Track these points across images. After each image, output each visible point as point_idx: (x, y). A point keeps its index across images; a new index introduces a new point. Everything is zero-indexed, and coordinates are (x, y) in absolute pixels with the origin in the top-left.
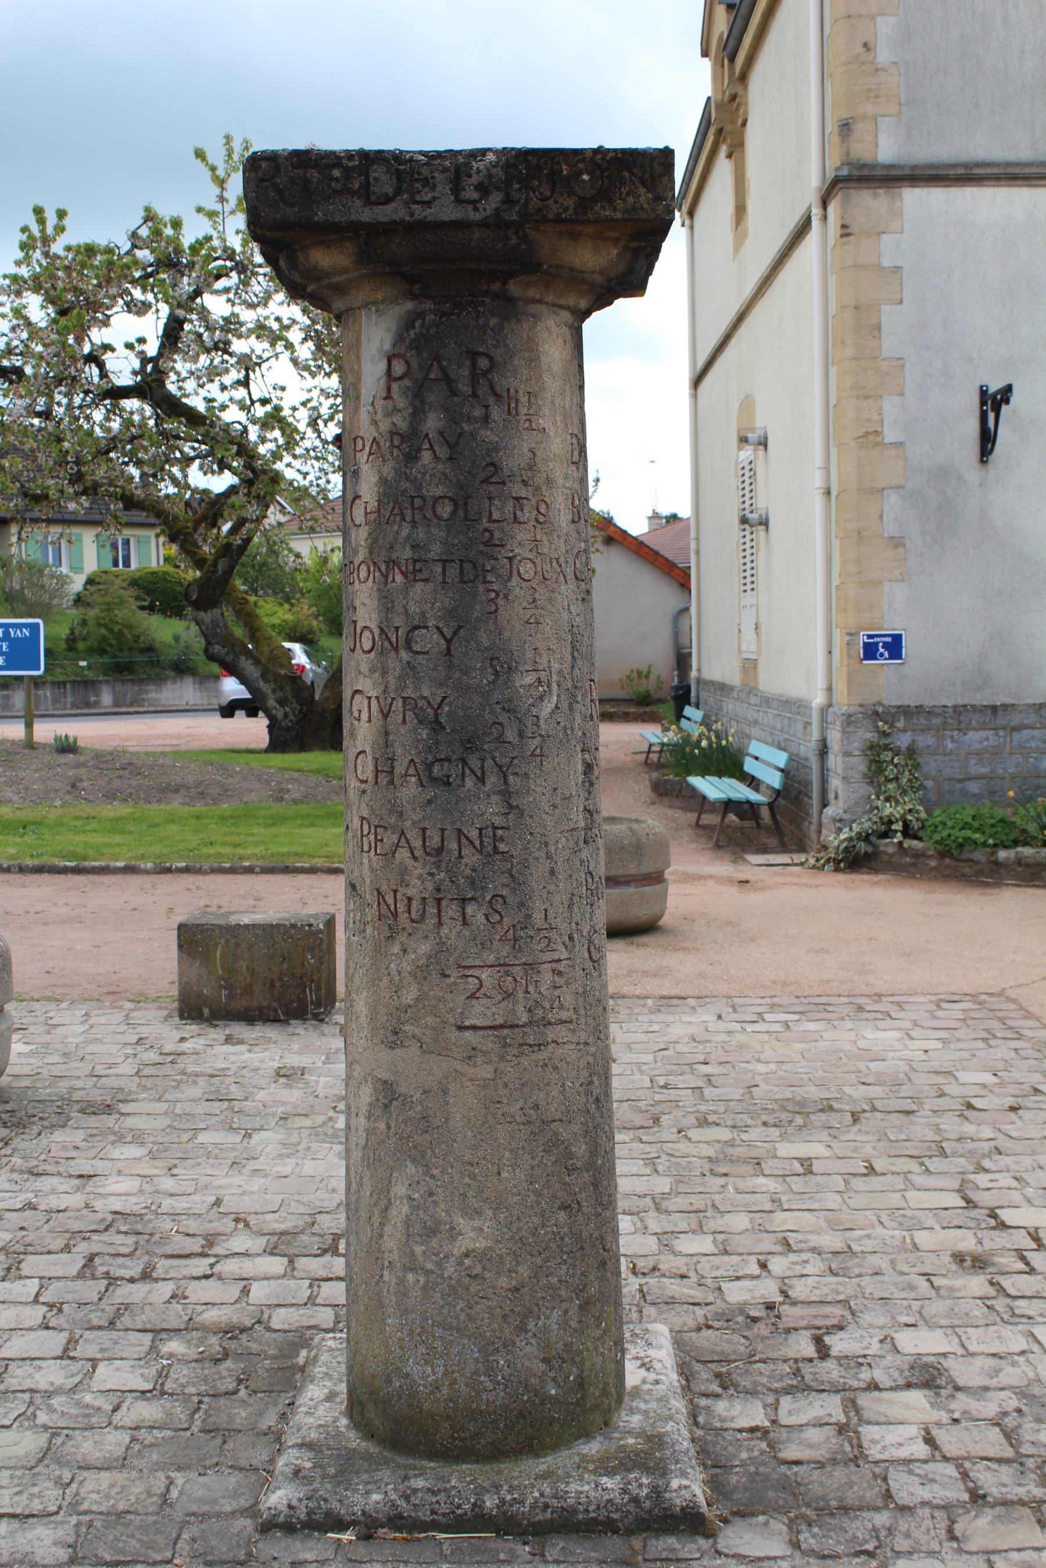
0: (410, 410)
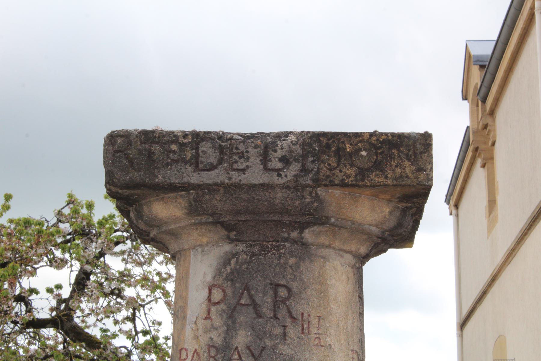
0: (225, 328)
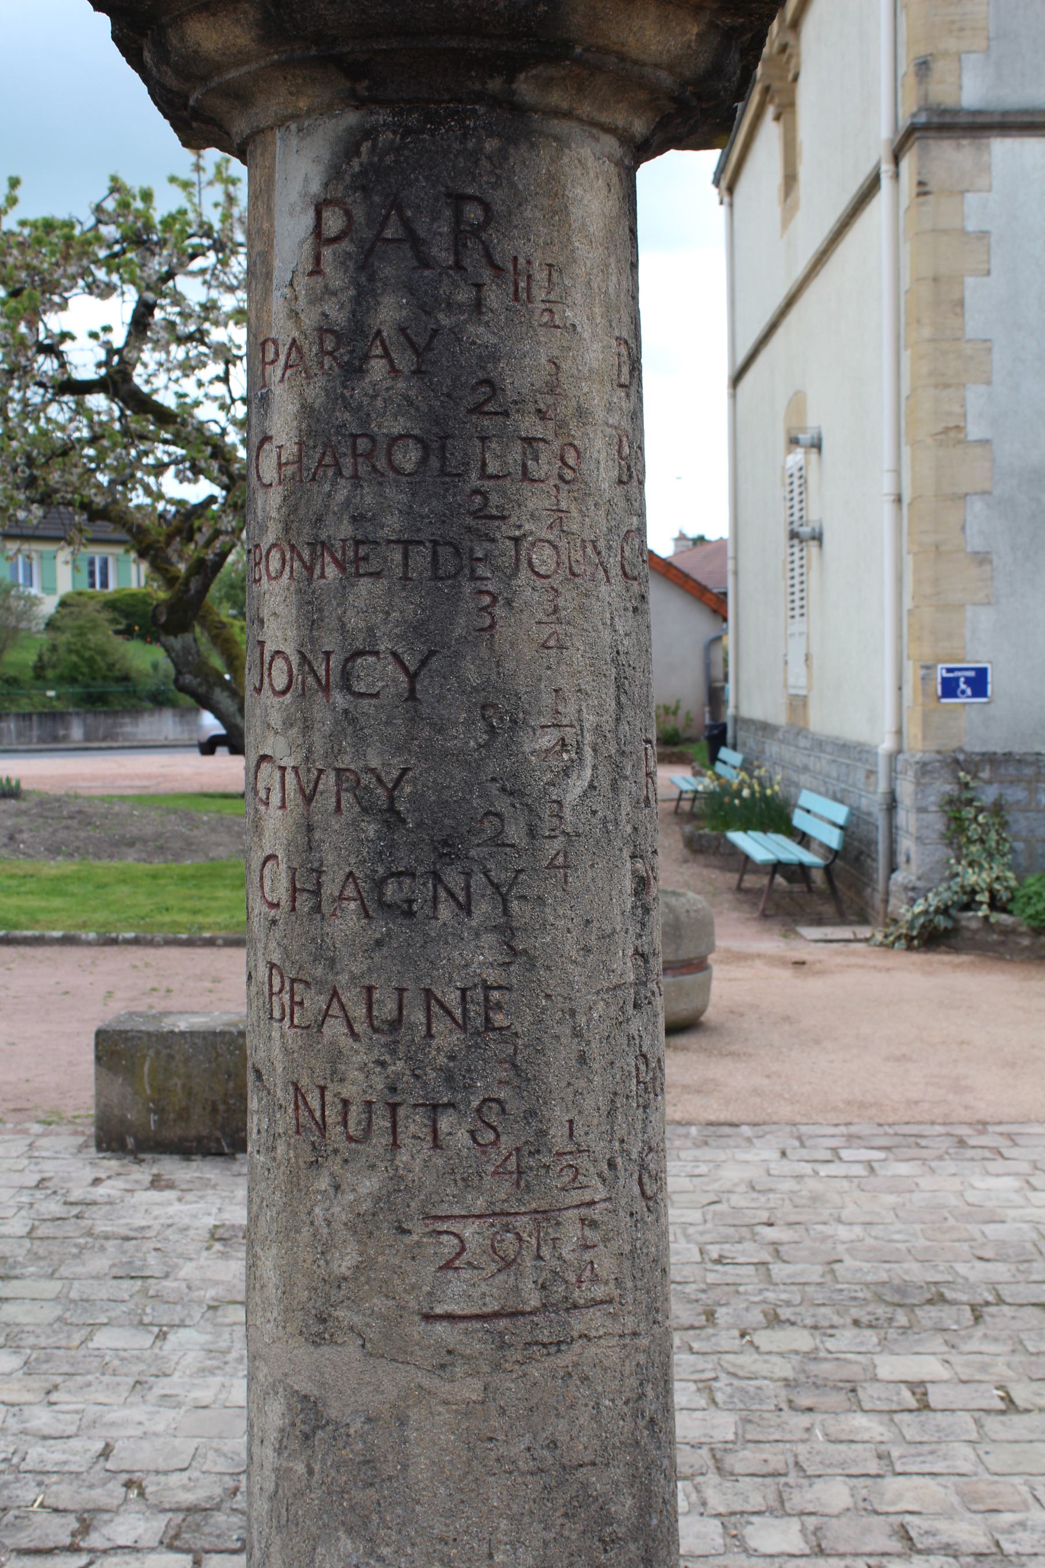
0: (352, 292)
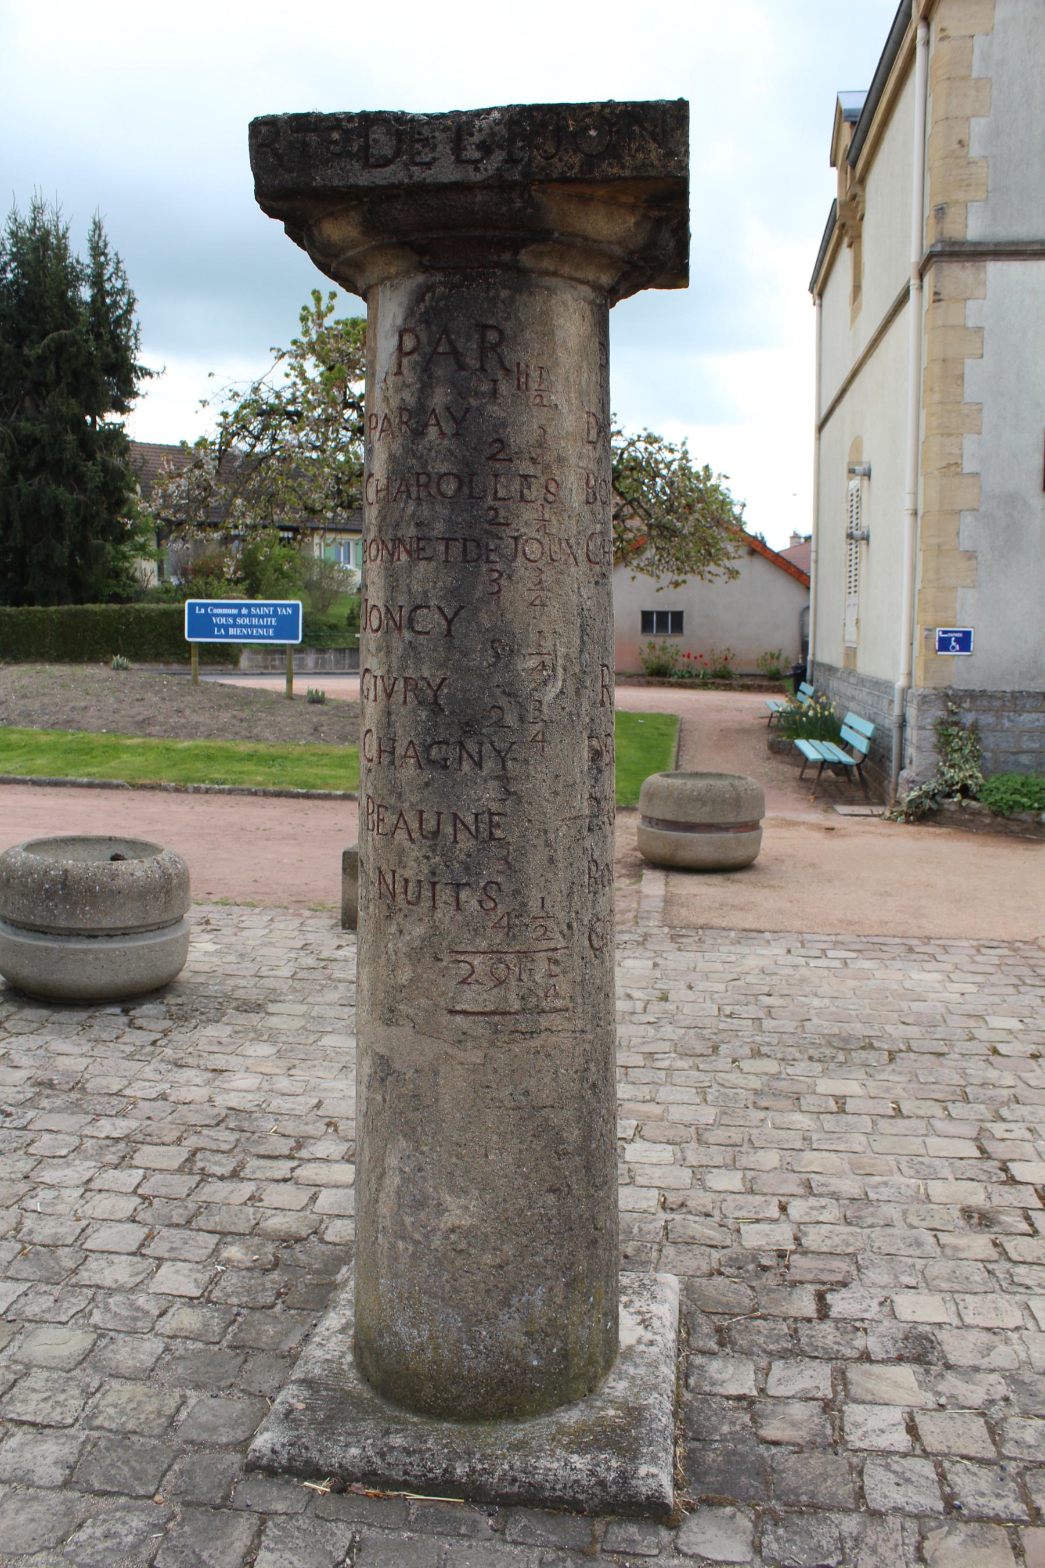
0: (418, 386)
